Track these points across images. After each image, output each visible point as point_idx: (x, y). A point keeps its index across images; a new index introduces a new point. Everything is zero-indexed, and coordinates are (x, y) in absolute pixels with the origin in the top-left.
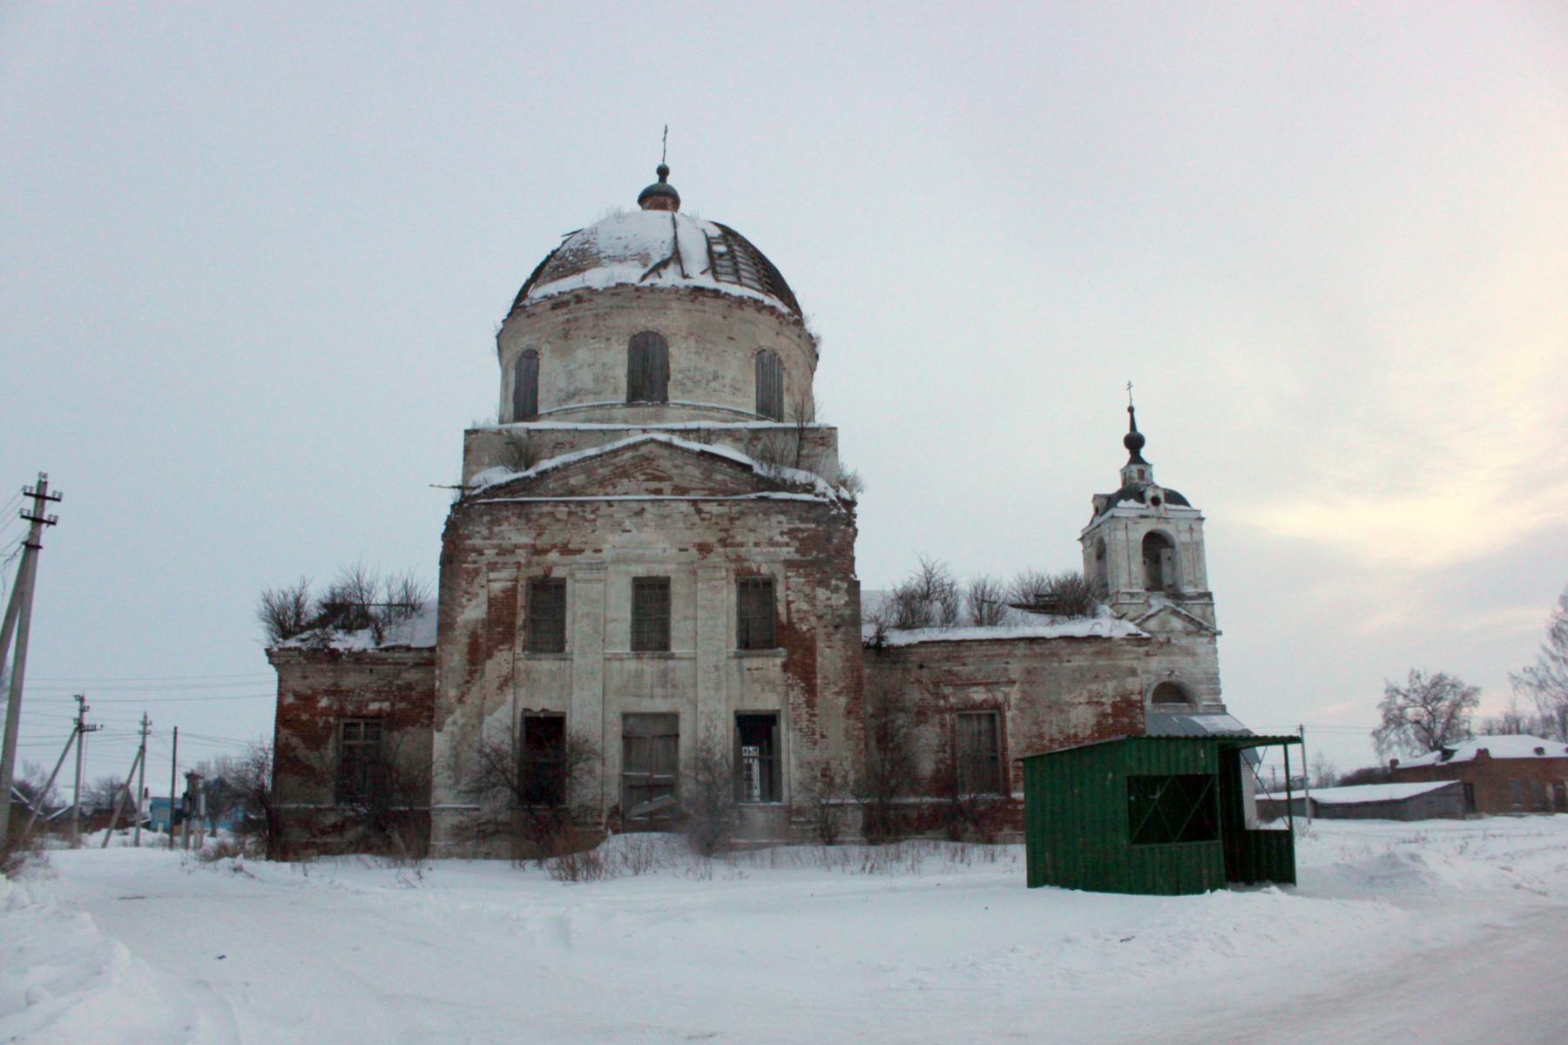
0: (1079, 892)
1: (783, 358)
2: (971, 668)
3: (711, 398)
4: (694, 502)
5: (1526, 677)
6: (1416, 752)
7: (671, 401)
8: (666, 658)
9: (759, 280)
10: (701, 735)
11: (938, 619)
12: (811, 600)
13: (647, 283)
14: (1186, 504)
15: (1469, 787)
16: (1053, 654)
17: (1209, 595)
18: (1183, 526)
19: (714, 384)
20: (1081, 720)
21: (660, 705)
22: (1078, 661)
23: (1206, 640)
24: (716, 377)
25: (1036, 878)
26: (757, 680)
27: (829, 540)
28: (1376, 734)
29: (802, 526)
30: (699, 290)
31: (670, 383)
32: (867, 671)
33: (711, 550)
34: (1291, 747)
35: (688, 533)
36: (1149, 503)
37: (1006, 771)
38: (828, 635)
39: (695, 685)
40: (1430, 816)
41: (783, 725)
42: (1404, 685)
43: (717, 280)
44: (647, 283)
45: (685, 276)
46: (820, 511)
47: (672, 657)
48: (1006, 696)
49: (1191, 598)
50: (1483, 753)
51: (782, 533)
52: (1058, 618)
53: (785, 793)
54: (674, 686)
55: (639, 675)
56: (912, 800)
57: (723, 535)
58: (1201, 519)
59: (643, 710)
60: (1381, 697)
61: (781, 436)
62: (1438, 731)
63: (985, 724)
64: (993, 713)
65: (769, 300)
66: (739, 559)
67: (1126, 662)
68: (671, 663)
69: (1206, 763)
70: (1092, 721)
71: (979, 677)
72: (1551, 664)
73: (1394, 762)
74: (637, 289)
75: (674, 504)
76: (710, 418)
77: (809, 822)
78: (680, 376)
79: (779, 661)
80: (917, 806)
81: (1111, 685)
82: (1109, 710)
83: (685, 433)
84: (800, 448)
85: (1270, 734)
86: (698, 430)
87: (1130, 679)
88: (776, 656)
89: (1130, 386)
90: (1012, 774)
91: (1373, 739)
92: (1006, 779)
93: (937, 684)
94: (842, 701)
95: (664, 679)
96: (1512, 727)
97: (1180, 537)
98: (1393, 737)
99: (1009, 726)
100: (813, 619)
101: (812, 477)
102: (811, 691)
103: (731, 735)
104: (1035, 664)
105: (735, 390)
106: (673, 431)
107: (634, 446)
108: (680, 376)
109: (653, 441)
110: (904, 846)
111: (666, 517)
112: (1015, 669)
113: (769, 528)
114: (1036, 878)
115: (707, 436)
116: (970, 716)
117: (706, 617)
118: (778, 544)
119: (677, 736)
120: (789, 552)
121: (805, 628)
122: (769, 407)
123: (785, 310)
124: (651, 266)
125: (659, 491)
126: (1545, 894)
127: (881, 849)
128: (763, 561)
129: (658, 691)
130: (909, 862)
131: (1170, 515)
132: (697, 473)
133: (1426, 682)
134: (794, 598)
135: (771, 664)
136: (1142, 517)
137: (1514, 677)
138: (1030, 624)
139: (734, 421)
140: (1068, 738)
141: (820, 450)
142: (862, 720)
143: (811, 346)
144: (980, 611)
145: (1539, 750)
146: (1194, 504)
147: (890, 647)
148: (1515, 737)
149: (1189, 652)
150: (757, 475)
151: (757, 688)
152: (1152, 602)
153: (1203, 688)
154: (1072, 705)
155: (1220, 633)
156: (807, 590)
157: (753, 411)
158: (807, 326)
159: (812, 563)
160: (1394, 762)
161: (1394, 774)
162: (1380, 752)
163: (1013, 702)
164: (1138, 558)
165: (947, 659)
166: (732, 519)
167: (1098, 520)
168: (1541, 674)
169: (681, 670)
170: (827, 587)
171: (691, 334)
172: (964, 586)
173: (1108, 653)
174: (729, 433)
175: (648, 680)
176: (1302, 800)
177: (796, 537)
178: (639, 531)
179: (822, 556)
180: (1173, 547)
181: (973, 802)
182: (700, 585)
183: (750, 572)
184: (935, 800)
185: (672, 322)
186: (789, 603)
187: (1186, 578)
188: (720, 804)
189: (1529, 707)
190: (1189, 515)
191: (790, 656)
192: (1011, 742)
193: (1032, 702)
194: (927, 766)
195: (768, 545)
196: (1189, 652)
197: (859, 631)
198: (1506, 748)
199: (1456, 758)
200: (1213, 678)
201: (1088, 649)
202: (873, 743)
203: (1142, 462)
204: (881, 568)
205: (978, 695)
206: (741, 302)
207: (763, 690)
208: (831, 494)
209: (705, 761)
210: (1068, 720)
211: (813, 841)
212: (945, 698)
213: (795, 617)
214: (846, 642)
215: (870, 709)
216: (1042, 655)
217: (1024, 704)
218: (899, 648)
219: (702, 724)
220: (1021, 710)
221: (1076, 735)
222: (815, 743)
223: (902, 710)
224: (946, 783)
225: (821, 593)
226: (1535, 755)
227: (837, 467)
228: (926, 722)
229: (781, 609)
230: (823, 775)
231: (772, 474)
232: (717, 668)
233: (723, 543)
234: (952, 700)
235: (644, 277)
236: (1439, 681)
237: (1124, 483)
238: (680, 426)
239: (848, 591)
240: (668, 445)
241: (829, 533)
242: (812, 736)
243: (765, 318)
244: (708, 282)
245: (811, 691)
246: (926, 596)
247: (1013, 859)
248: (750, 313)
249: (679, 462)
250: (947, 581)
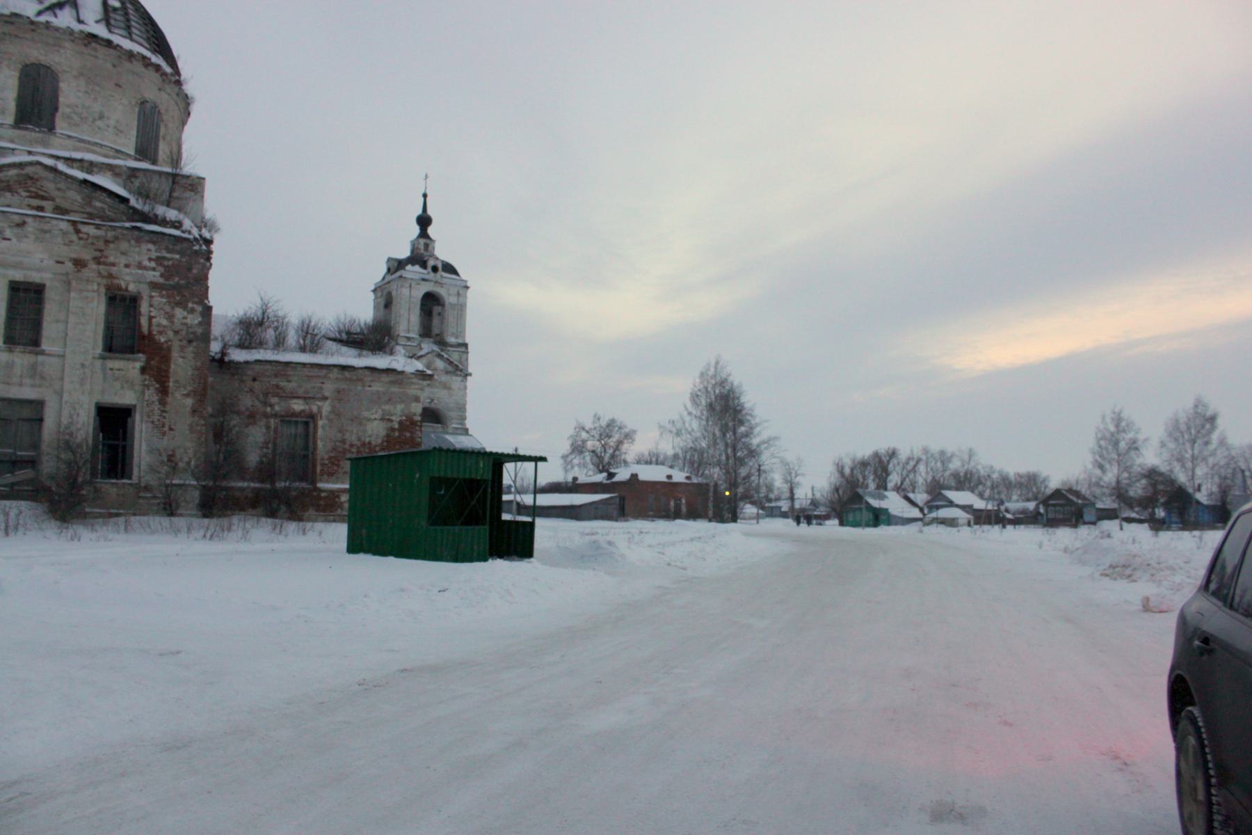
0: (391, 559)
1: (163, 111)
2: (293, 385)
3: (96, 131)
4: (74, 223)
5: (669, 426)
6: (591, 473)
7: (58, 130)
8: (37, 354)
9: (148, 40)
10: (65, 421)
11: (271, 344)
12: (170, 317)
13: (43, 19)
15: (622, 499)
16: (359, 380)
17: (466, 345)
18: (453, 291)
19: (99, 123)
20: (375, 431)
21: (28, 393)
22: (377, 387)
23: (459, 379)
24: (101, 117)
25: (355, 546)
26: (116, 379)
27: (190, 270)
28: (564, 457)
29: (168, 255)
30: (93, 37)
31: (58, 115)
32: (210, 379)
33: (85, 266)
34: (540, 464)
35: (66, 248)
37: (314, 466)
38: (182, 348)
39: (62, 379)
40: (596, 518)
41: (138, 417)
42: (588, 424)
43: (110, 31)
44: (43, 19)
45: (80, 21)
46: (185, 245)
47: (42, 353)
48: (320, 408)
49: (452, 346)
50: (634, 476)
51: (150, 259)
52: (365, 352)
53: (135, 472)
54: (42, 378)
55: (10, 366)
56: (240, 484)
57: (98, 254)
58: (467, 287)
59: (11, 396)
60: (571, 432)
61: (156, 177)
62: (606, 459)
63: (301, 429)
64: (309, 420)
65: (156, 59)
66: (110, 276)
67: (412, 391)
68: (40, 358)
69: (482, 471)
70: (383, 433)
71: (301, 392)
72: (687, 418)
73: (575, 479)
74: (32, 23)
75: (54, 222)
76: (94, 152)
77: (155, 497)
78: (68, 110)
79: (138, 365)
80: (242, 490)
81: (400, 407)
82: (396, 426)
83: (69, 161)
84: (172, 191)
85: (528, 454)
86: (81, 161)
87: (414, 404)
88: (135, 360)
89: (426, 177)
90: (319, 469)
91: (561, 461)
92: (314, 472)
93: (266, 395)
94: (189, 402)
95: (34, 371)
96: (653, 459)
97: (450, 299)
98: (576, 461)
99: (320, 432)
100: (171, 334)
101: (181, 217)
102: (164, 391)
103: (92, 421)
104: (343, 386)
105: (119, 131)
106: (57, 158)
107: (21, 165)
108: (68, 110)
109: (39, 163)
110: (235, 520)
111: (46, 232)
112: (329, 388)
113: (139, 253)
114: (355, 546)
115: (90, 167)
116: (290, 422)
117: (75, 323)
118: (145, 268)
119: (41, 420)
120: (155, 276)
121: (163, 340)
122: (146, 150)
123: (168, 70)
124: (47, 4)
125: (41, 209)
126: (685, 569)
127: (215, 521)
128: (130, 281)
129: (27, 381)
130: (240, 533)
131: (445, 281)
132: (79, 198)
133: (604, 423)
134: (155, 314)
135: (132, 367)
136: (424, 280)
137: (661, 427)
138: (342, 355)
139: (115, 158)
140: (364, 444)
141: (188, 194)
142: (202, 417)
143: (185, 104)
145: (669, 477)
146: (463, 276)
147: (231, 362)
148: (653, 467)
149: (446, 387)
150: (134, 209)
151: (118, 384)
153: (453, 414)
154: (369, 420)
156: (168, 308)
157: (132, 153)
158: (184, 87)
159: (174, 287)
160: (575, 479)
161: (574, 487)
162: (566, 471)
163: (324, 413)
165: (276, 376)
166: (107, 242)
167: (389, 278)
168: (679, 425)
169: (49, 365)
170: (185, 308)
171: (81, 74)
173: (399, 383)
174: (110, 168)
175: (18, 370)
176: (510, 502)
177: (161, 265)
178: (19, 239)
179: (182, 282)
181: (288, 489)
182: (73, 294)
183: (119, 288)
184: (257, 485)
185: (64, 60)
186: (151, 318)
188: (80, 479)
189: (668, 447)
191: (148, 361)
192: (320, 444)
193: (338, 415)
194: (252, 458)
195: (137, 268)
196: (446, 387)
197: (208, 347)
198: (651, 474)
199: (616, 479)
200: (462, 408)
201: (385, 378)
202: (211, 437)
204: (230, 295)
205: (298, 406)
206: (131, 55)
207: (122, 388)
208: (195, 232)
209: (67, 442)
210: (365, 431)
211: (157, 513)
212: (271, 406)
213: (155, 330)
214: (197, 355)
215: (210, 410)
216: (350, 380)
217: (332, 416)
218: (238, 363)
219: (65, 413)
220: (330, 420)
221: (370, 443)
222: (164, 434)
223: (238, 413)
224: (267, 471)
225: (179, 313)
226: (665, 480)
227: (201, 209)
228: (254, 423)
229: (144, 322)
230: (169, 460)
231: (146, 209)
232: (83, 365)
233: (98, 261)
234: (277, 408)
235: (40, 13)
236: (611, 424)
237: (412, 252)
238: (66, 154)
239: (202, 314)
240: (54, 170)
241: (189, 264)
242: (162, 428)
243: (151, 73)
244: (101, 31)
245: (164, 391)
246: (260, 323)
247: (339, 532)
248: (138, 67)
249: (62, 185)
250: (280, 314)
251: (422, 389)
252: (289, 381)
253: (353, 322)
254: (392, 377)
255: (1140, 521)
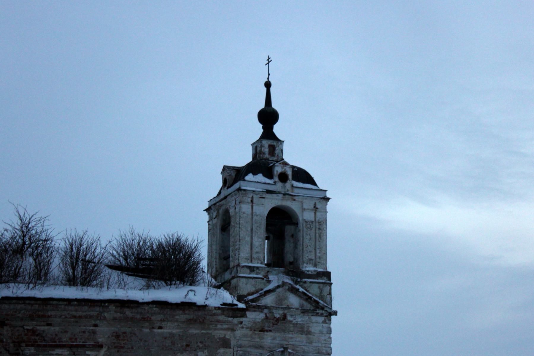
14: (313, 183)
16: (144, 319)
17: (328, 275)
18: (308, 204)
22: (170, 329)
23: (321, 319)
36: (276, 179)
49: (310, 276)
71: (65, 338)
89: (269, 61)
112: (104, 332)
131: (296, 192)
136: (268, 192)
138: (122, 285)
144: (74, 268)
146: (321, 185)
149: (304, 330)
152: (271, 277)
155: (335, 313)
164: (261, 232)
165: (32, 318)
172: (59, 242)
180: (296, 224)
187: (306, 258)
190: (315, 194)
196: (304, 330)
201: (181, 316)
203: (274, 137)
216: (132, 319)
237: (255, 156)
246: (19, 251)
251: (233, 330)
252: (49, 325)
253: (143, 244)
254: (189, 315)
255: (249, 294)
